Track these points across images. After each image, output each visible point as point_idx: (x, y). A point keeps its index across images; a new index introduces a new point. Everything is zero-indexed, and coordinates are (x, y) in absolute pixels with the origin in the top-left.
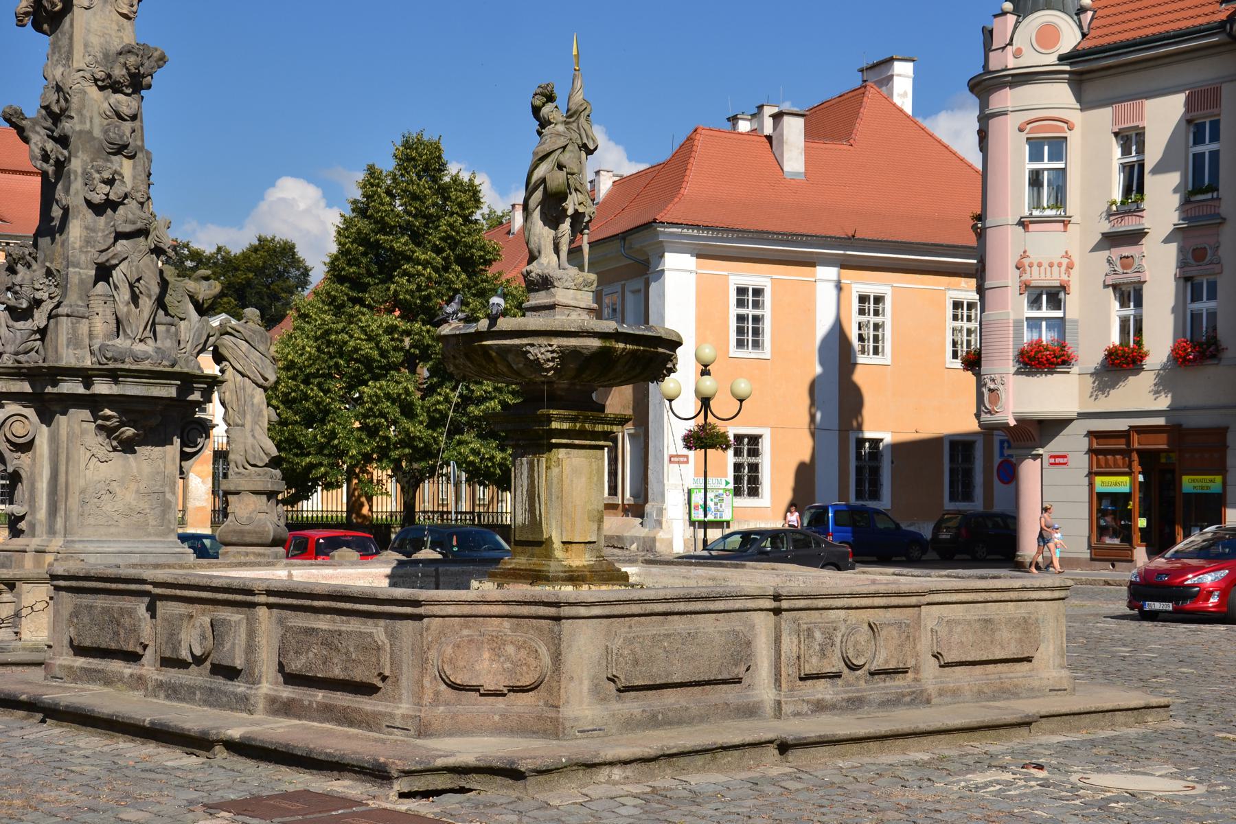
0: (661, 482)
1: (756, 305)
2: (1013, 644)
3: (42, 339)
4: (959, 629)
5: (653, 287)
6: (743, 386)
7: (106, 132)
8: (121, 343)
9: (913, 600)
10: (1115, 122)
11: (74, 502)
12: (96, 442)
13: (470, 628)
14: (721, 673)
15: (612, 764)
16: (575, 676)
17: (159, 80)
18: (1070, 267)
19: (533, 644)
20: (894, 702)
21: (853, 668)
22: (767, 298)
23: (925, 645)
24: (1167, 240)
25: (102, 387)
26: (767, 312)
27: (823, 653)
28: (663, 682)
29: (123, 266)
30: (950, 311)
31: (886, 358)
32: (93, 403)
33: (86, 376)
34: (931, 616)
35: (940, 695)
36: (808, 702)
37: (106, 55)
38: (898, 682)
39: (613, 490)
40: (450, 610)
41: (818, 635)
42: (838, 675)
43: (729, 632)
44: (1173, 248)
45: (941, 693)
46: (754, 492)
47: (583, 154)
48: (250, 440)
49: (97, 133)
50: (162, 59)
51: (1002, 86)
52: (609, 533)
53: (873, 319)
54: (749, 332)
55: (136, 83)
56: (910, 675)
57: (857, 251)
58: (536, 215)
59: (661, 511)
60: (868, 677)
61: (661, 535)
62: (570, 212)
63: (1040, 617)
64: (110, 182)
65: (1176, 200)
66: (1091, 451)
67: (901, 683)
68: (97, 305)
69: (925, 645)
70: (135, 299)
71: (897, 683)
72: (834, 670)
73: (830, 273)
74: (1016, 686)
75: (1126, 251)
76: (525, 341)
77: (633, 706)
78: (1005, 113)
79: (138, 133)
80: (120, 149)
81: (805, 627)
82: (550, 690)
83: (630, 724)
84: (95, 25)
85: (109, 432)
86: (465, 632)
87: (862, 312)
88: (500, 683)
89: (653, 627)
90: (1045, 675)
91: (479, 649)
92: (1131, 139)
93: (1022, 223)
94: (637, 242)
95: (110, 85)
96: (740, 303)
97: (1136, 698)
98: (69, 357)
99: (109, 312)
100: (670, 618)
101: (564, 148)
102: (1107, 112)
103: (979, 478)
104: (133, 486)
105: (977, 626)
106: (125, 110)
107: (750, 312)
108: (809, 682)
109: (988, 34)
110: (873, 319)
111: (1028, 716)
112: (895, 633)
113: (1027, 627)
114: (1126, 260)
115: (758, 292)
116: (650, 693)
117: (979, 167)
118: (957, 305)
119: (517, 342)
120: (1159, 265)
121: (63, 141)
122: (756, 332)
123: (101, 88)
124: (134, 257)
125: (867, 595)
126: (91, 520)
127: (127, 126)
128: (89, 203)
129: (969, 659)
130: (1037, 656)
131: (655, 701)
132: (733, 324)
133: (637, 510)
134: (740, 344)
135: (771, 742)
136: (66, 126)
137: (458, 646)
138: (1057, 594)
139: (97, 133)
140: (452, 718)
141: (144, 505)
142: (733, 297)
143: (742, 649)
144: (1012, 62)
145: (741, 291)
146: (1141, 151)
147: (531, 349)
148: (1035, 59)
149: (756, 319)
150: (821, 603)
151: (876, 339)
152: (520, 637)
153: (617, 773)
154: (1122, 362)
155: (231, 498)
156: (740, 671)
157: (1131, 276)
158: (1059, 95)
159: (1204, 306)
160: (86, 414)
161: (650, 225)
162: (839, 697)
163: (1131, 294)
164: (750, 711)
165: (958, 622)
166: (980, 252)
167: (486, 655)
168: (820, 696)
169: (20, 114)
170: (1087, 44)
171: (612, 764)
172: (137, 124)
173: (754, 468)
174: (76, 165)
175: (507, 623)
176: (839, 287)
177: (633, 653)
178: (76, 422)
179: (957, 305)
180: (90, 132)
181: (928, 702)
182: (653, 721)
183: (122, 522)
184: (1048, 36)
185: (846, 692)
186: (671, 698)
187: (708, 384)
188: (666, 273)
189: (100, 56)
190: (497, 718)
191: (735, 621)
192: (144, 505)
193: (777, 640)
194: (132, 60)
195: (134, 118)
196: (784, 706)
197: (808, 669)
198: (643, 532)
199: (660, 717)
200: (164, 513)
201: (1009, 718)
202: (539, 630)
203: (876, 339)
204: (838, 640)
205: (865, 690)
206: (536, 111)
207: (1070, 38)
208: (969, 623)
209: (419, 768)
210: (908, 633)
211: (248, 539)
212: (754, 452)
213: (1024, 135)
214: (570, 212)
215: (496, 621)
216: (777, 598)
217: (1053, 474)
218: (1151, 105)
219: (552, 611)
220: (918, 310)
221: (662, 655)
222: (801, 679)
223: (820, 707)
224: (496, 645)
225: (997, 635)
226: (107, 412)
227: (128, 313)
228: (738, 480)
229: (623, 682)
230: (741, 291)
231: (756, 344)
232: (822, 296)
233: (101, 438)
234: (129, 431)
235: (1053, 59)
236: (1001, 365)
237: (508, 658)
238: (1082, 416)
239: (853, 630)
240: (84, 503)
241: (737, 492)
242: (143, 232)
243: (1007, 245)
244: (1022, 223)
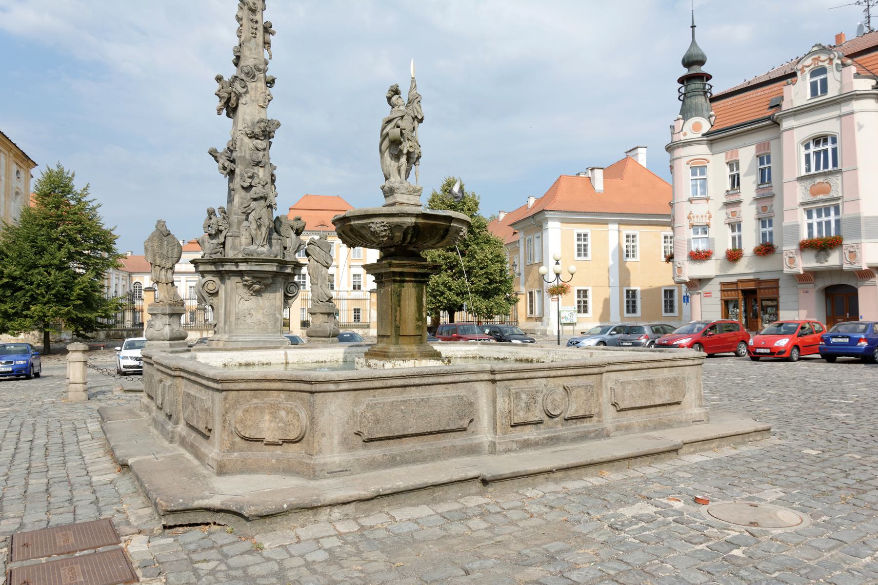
0: (548, 308)
1: (585, 240)
2: (667, 394)
3: (224, 247)
4: (630, 387)
5: (544, 234)
6: (573, 268)
7: (251, 156)
8: (253, 247)
9: (596, 370)
10: (727, 158)
11: (233, 318)
12: (243, 291)
13: (258, 398)
14: (448, 425)
15: (332, 505)
16: (327, 433)
17: (278, 134)
18: (710, 217)
19: (297, 410)
20: (584, 437)
21: (551, 417)
22: (589, 237)
23: (605, 397)
24: (750, 204)
25: (243, 267)
26: (589, 242)
27: (528, 407)
28: (400, 434)
29: (253, 213)
30: (663, 240)
31: (638, 258)
32: (241, 274)
33: (236, 262)
34: (610, 380)
35: (617, 430)
36: (516, 442)
37: (253, 124)
38: (586, 425)
39: (531, 312)
40: (242, 386)
41: (524, 396)
42: (540, 422)
43: (455, 397)
44: (754, 207)
45: (618, 428)
46: (585, 311)
47: (416, 122)
48: (320, 290)
49: (248, 157)
50: (279, 125)
51: (678, 147)
52: (823, 320)
53: (632, 244)
54: (582, 250)
55: (267, 135)
56: (595, 419)
57: (626, 218)
58: (387, 154)
59: (549, 320)
60: (564, 422)
61: (548, 329)
62: (405, 151)
63: (686, 376)
64: (251, 177)
65: (754, 187)
66: (722, 291)
67: (588, 424)
68: (243, 231)
69: (605, 397)
70: (259, 227)
71: (585, 424)
72: (536, 419)
73: (616, 226)
74: (670, 421)
75: (733, 209)
76: (369, 221)
77: (376, 452)
78: (680, 158)
79: (266, 156)
80: (257, 164)
81: (514, 391)
82: (308, 443)
83: (372, 465)
84: (248, 111)
85: (249, 287)
86: (255, 401)
87: (627, 241)
88: (276, 437)
89: (392, 397)
90: (689, 412)
91: (261, 413)
92: (733, 164)
93: (690, 201)
94: (538, 218)
95: (253, 136)
96: (579, 240)
97: (748, 425)
98: (230, 254)
99: (248, 234)
100: (408, 389)
101: (402, 117)
102: (723, 155)
103: (676, 304)
104: (261, 311)
105: (643, 384)
106: (260, 147)
107: (582, 243)
108: (518, 428)
109: (672, 127)
110: (632, 244)
111: (675, 445)
112: (583, 393)
113: (675, 383)
114: (734, 214)
115: (585, 235)
116: (392, 441)
117: (671, 183)
118: (666, 237)
119: (365, 221)
120: (748, 213)
121: (233, 161)
122: (585, 250)
123: (250, 138)
124: (258, 210)
125: (562, 368)
126: (241, 327)
127: (261, 154)
128: (243, 187)
129: (637, 405)
130: (685, 401)
131: (395, 448)
132: (576, 248)
133: (540, 319)
134: (579, 255)
135: (477, 478)
136: (234, 154)
137: (247, 411)
138: (696, 362)
139: (248, 157)
140: (243, 461)
141: (266, 320)
142: (576, 237)
143: (467, 409)
144: (682, 138)
145: (579, 235)
146: (738, 169)
147: (371, 225)
148: (691, 136)
149: (585, 245)
150: (526, 375)
151: (633, 251)
152: (290, 404)
153: (337, 513)
154: (734, 256)
155: (563, 321)
156: (465, 423)
157: (736, 219)
158: (702, 150)
159: (767, 229)
160: (238, 279)
161: (542, 212)
162: (541, 437)
163: (735, 226)
164: (473, 450)
165: (628, 383)
166: (672, 217)
167: (267, 417)
168: (526, 437)
169: (216, 151)
170: (713, 129)
171: (332, 505)
172: (266, 153)
173: (585, 302)
174: (237, 171)
175: (283, 395)
176: (619, 231)
177: (375, 414)
178: (233, 283)
179: (666, 237)
180: (244, 157)
181: (608, 436)
182: (393, 462)
183: (256, 327)
184: (697, 127)
185: (546, 433)
186: (408, 446)
187: (558, 268)
188: (549, 230)
189: (250, 124)
190: (274, 461)
191: (461, 391)
192: (266, 320)
193: (494, 401)
194: (262, 124)
195: (264, 150)
196: (498, 446)
197: (516, 420)
198: (542, 328)
199: (398, 458)
200: (275, 323)
201: (662, 447)
202: (302, 399)
203: (633, 251)
204: (540, 400)
205: (561, 431)
206: (389, 99)
207: (706, 127)
208: (637, 382)
209: (180, 508)
210: (593, 392)
211: (319, 334)
212: (585, 296)
213: (689, 166)
214: (405, 151)
215: (276, 393)
216: (493, 372)
217: (706, 300)
218: (741, 151)
219: (307, 387)
220: (650, 240)
221: (400, 415)
222: (512, 426)
223: (526, 445)
224: (274, 409)
225: (657, 390)
226: (246, 278)
227: (256, 234)
228: (579, 307)
229: (366, 436)
230: (579, 235)
231: (585, 255)
232: (612, 235)
233: (245, 290)
234: (257, 287)
235: (700, 135)
236: (682, 258)
237: (281, 420)
238: (717, 276)
239: (552, 392)
240: (237, 319)
241: (579, 312)
242: (264, 198)
243: (683, 211)
244: (690, 201)
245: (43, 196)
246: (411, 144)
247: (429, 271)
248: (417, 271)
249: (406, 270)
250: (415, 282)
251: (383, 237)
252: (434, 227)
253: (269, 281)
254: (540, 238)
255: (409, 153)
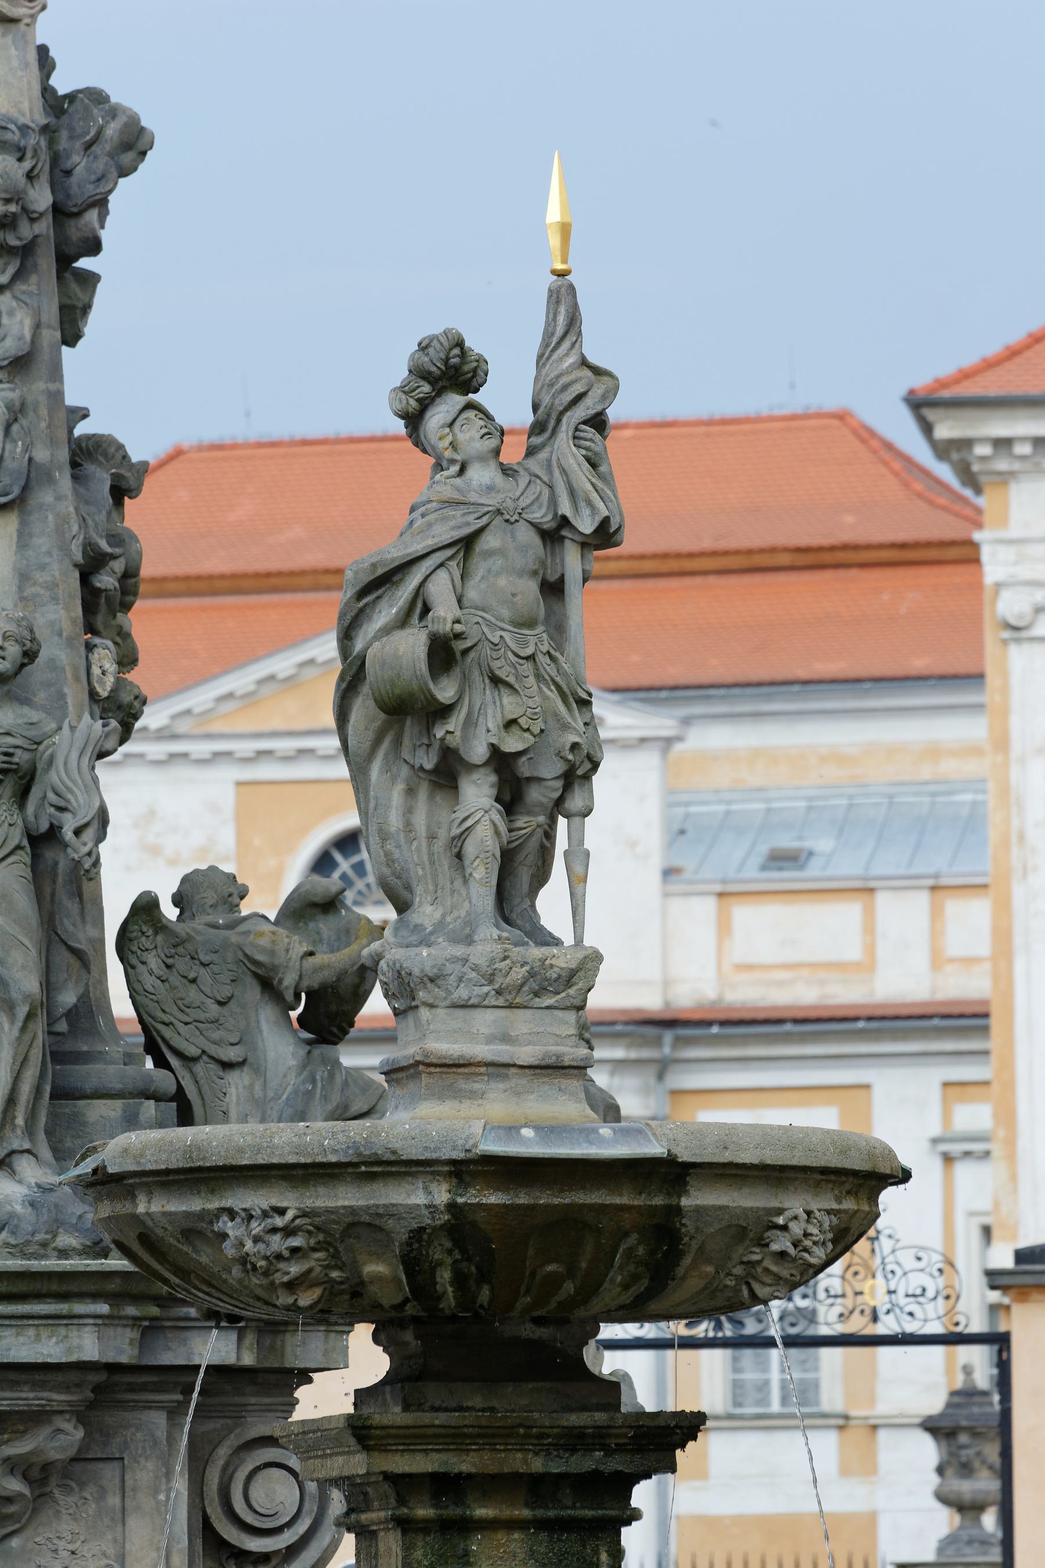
62: (479, 752)
119: (196, 1204)
147: (226, 1225)
245: (371, 956)
246: (510, 705)
247: (615, 1464)
248: (537, 1465)
249: (465, 1464)
250: (542, 1525)
251: (291, 1286)
252: (571, 1223)
253: (62, 1439)
254: (941, 1458)
255: (501, 762)
